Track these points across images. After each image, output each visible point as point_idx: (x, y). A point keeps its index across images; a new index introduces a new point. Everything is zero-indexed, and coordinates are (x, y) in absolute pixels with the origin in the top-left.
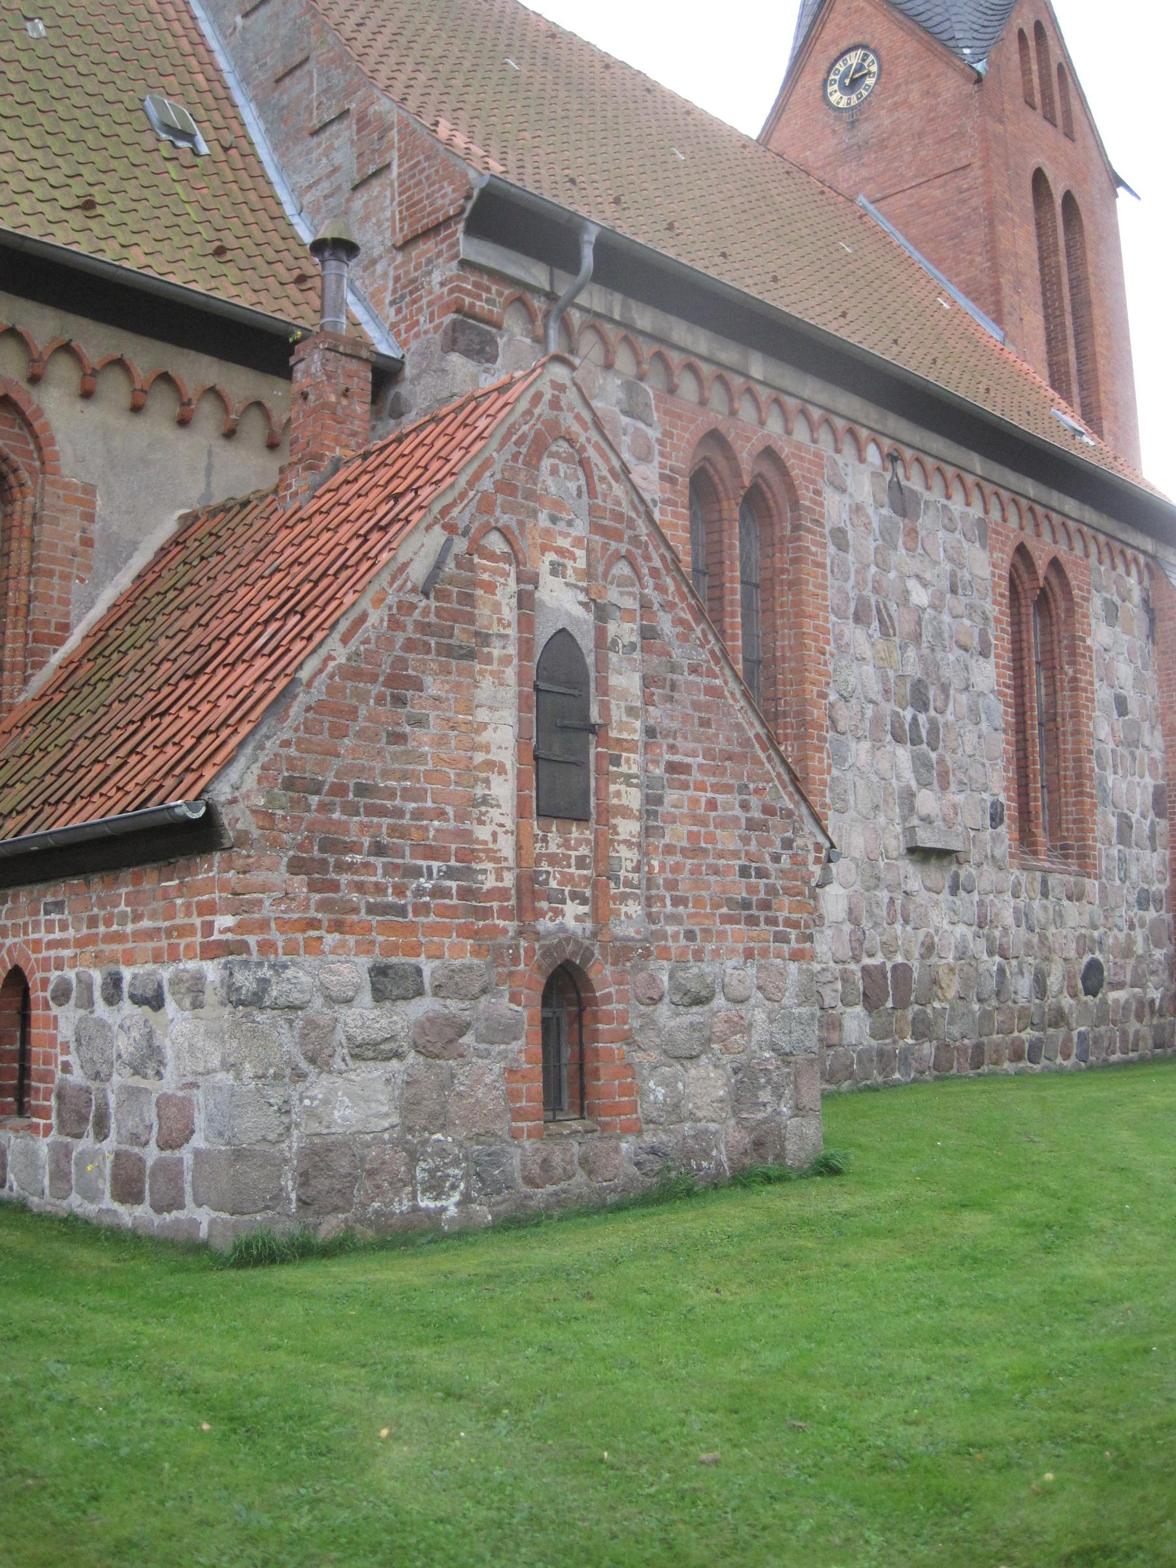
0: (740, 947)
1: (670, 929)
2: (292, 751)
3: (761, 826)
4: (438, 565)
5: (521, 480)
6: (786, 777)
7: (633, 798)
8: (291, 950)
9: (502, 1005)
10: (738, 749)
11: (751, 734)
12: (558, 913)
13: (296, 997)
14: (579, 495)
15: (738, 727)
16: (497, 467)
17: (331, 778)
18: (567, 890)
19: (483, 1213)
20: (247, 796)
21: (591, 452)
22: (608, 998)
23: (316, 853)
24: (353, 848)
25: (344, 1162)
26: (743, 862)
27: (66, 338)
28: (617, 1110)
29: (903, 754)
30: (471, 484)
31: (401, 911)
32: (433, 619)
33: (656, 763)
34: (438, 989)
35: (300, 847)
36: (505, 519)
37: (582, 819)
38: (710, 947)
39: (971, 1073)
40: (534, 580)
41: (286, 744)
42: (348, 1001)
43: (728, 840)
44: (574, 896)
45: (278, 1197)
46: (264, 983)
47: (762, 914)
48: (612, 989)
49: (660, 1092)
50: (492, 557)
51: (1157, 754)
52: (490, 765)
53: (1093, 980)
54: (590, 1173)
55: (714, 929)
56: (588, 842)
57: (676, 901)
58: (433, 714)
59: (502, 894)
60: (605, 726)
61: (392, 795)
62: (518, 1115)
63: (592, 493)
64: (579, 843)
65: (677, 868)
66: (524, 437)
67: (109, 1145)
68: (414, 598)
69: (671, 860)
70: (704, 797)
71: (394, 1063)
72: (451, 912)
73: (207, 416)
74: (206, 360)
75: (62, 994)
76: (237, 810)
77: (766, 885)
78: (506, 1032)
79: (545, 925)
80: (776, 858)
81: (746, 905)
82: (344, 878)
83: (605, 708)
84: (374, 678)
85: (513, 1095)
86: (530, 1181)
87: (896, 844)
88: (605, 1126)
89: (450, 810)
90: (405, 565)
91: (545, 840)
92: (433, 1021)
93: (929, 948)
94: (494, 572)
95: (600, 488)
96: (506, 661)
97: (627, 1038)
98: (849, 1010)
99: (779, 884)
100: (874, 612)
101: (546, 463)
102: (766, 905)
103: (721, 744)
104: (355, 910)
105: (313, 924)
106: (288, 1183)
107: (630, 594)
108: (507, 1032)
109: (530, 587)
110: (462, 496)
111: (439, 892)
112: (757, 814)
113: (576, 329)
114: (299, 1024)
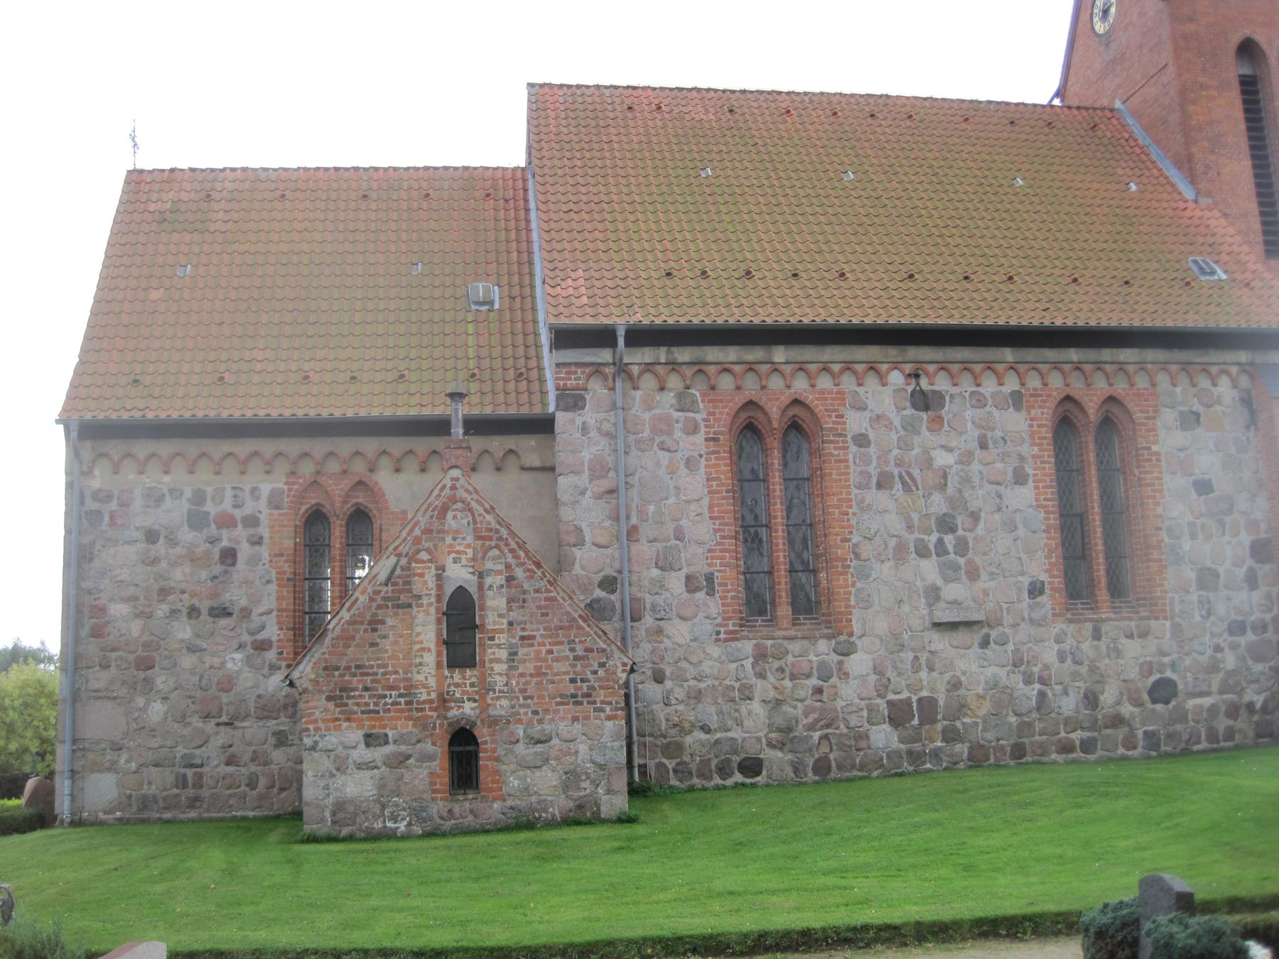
0: (570, 716)
1: (522, 711)
2: (327, 656)
4: (393, 572)
5: (436, 526)
6: (601, 633)
7: (503, 654)
8: (328, 729)
9: (428, 747)
11: (576, 615)
13: (330, 747)
14: (469, 524)
15: (568, 613)
16: (422, 524)
17: (344, 664)
19: (418, 830)
20: (307, 675)
21: (474, 504)
23: (338, 693)
26: (572, 676)
27: (383, 448)
28: (491, 790)
30: (409, 534)
31: (378, 712)
32: (390, 594)
33: (514, 637)
34: (395, 742)
35: (331, 691)
36: (427, 545)
37: (472, 665)
38: (548, 717)
39: (1012, 763)
40: (443, 568)
41: (324, 653)
42: (354, 747)
43: (559, 667)
44: (469, 700)
45: (323, 820)
46: (316, 743)
47: (585, 700)
48: (488, 738)
50: (422, 562)
52: (423, 649)
54: (475, 816)
55: (551, 709)
56: (476, 676)
57: (525, 698)
59: (431, 701)
60: (483, 625)
61: (372, 667)
62: (434, 791)
63: (475, 522)
64: (471, 677)
65: (527, 683)
66: (436, 507)
68: (380, 588)
69: (523, 680)
70: (544, 650)
71: (376, 771)
72: (402, 711)
79: (452, 713)
80: (595, 672)
81: (574, 696)
82: (350, 702)
83: (482, 617)
84: (362, 623)
85: (432, 783)
86: (441, 818)
89: (400, 671)
90: (376, 575)
91: (452, 677)
94: (424, 568)
95: (479, 519)
96: (430, 604)
97: (497, 759)
98: (874, 728)
100: (897, 478)
101: (450, 515)
103: (556, 622)
104: (356, 713)
105: (337, 719)
106: (328, 814)
108: (431, 758)
109: (441, 572)
110: (404, 540)
112: (580, 653)
113: (636, 376)
114: (332, 757)
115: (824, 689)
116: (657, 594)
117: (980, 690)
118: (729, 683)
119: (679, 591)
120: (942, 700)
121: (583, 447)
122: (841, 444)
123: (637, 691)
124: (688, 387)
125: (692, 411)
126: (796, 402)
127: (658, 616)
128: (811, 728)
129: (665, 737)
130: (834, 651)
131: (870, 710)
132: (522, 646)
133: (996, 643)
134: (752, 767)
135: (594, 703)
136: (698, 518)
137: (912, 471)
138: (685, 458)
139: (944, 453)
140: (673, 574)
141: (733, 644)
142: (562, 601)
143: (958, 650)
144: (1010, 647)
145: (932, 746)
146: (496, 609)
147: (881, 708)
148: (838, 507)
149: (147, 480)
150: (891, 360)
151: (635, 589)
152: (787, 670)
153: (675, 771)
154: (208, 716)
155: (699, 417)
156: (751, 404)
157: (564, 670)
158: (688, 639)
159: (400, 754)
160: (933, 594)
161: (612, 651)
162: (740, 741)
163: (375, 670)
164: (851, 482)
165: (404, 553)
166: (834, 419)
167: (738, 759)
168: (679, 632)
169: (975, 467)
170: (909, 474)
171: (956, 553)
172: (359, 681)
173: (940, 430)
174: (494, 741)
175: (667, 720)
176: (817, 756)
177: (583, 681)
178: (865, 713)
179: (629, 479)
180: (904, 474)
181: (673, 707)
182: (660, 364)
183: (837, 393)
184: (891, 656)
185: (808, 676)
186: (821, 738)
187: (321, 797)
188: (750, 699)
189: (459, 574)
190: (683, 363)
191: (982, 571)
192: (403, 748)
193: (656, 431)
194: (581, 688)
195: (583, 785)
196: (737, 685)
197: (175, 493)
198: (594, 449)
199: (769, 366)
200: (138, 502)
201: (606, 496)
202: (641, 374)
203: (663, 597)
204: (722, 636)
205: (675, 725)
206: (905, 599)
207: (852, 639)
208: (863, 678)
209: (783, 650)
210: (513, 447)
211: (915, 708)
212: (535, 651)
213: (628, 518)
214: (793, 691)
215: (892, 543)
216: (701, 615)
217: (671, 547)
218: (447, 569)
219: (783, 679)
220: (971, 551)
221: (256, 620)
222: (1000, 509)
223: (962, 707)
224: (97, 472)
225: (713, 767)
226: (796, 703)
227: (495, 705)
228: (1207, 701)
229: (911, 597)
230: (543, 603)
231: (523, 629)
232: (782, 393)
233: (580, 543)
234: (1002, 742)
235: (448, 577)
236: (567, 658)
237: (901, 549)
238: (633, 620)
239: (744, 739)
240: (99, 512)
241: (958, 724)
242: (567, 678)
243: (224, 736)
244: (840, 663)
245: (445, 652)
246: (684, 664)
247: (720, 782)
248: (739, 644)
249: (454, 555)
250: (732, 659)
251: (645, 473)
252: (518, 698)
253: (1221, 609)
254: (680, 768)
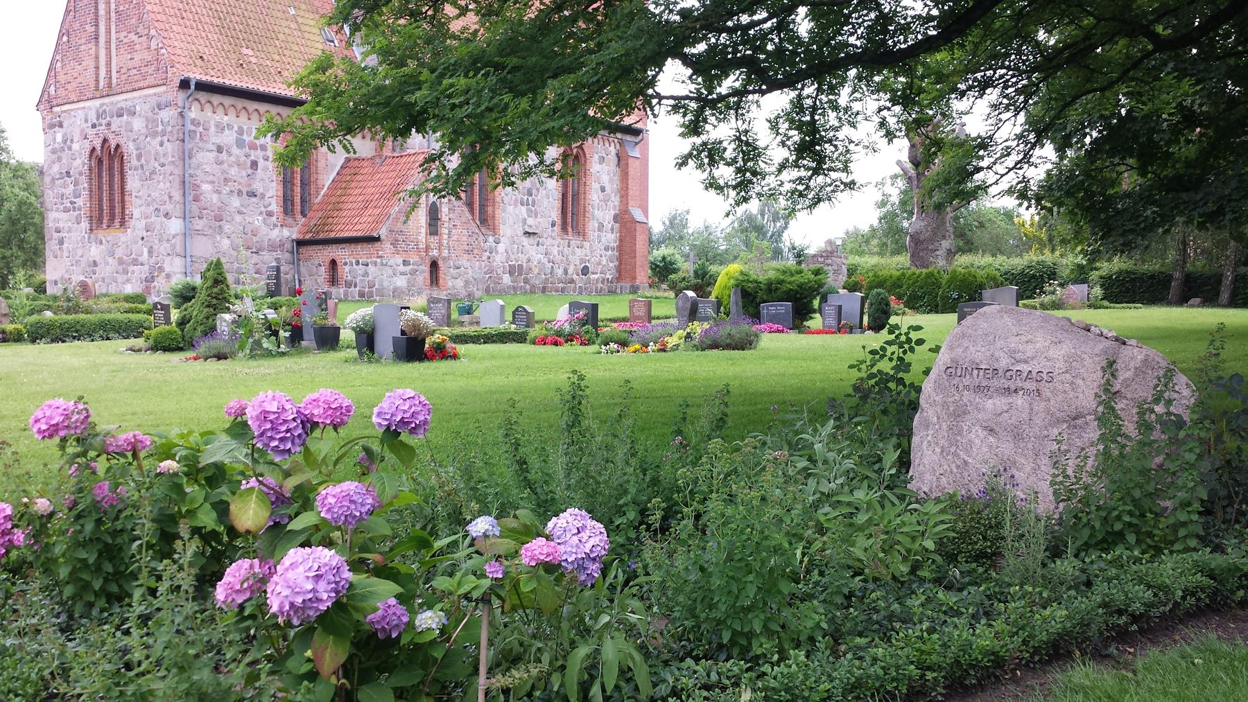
7: (446, 231)
29: (524, 209)
51: (617, 203)
53: (585, 271)
67: (358, 289)
75: (345, 264)
78: (423, 272)
87: (520, 232)
92: (412, 270)
93: (529, 261)
103: (464, 220)
154: (248, 248)
197: (230, 127)
200: (213, 129)
221: (267, 200)
224: (193, 109)
228: (596, 276)
243: (255, 258)
253: (603, 240)
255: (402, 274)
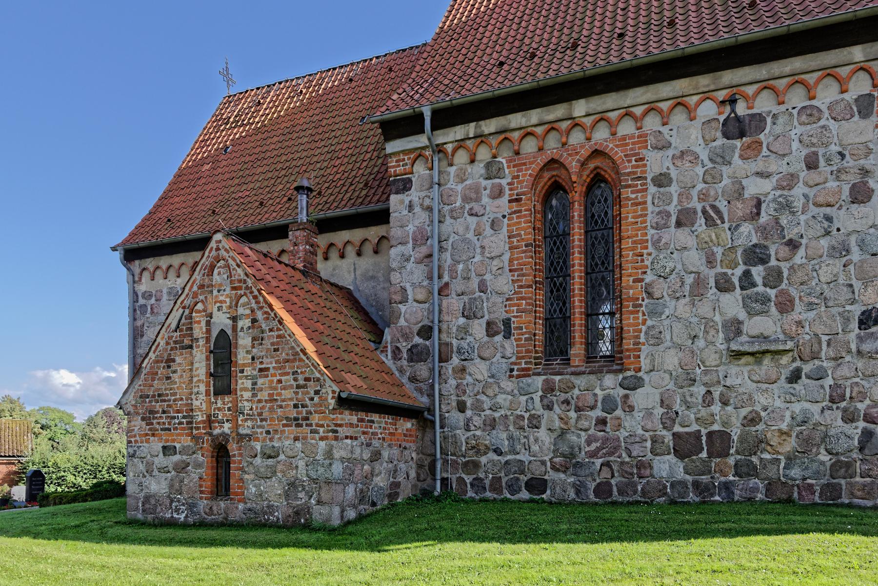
0: (292, 436)
1: (259, 430)
2: (142, 387)
3: (305, 387)
7: (248, 384)
10: (292, 357)
12: (222, 427)
18: (225, 419)
22: (234, 456)
24: (157, 412)
25: (153, 501)
26: (295, 402)
28: (236, 494)
30: (190, 290)
35: (144, 414)
36: (201, 297)
37: (229, 392)
38: (277, 436)
41: (140, 385)
43: (288, 394)
45: (137, 509)
47: (304, 423)
49: (254, 490)
57: (262, 420)
58: (178, 369)
61: (167, 395)
62: (201, 492)
64: (228, 402)
65: (263, 408)
68: (172, 334)
69: (260, 405)
70: (275, 379)
72: (183, 429)
73: (350, 251)
74: (344, 232)
76: (127, 406)
77: (306, 411)
80: (312, 399)
81: (296, 419)
82: (155, 421)
84: (162, 362)
85: (201, 486)
88: (232, 499)
89: (184, 397)
90: (170, 324)
91: (216, 403)
95: (233, 273)
97: (242, 469)
98: (658, 458)
99: (312, 410)
100: (700, 214)
101: (216, 271)
102: (307, 419)
105: (147, 435)
107: (247, 308)
109: (209, 318)
111: (180, 423)
112: (302, 382)
115: (608, 420)
116: (462, 339)
117: (784, 427)
118: (520, 413)
119: (481, 336)
120: (735, 433)
121: (408, 221)
122: (639, 187)
123: (442, 418)
124: (495, 157)
125: (499, 178)
126: (597, 153)
127: (462, 357)
128: (593, 454)
129: (465, 457)
130: (620, 385)
131: (654, 441)
132: (261, 377)
133: (808, 377)
134: (537, 485)
135: (311, 425)
136: (500, 271)
137: (717, 204)
138: (490, 220)
139: (759, 180)
140: (476, 321)
141: (524, 380)
142: (288, 338)
143: (760, 385)
144: (829, 381)
145: (723, 479)
146: (245, 347)
147: (666, 441)
148: (633, 249)
149: (169, 283)
150: (700, 90)
151: (444, 336)
152: (573, 402)
153: (471, 484)
155: (504, 182)
156: (553, 162)
157: (289, 397)
158: (486, 375)
159: (183, 461)
160: (734, 328)
161: (324, 380)
162: (527, 463)
163: (169, 397)
164: (648, 224)
165: (187, 306)
166: (634, 163)
167: (526, 479)
168: (479, 370)
169: (799, 190)
170: (713, 207)
171: (765, 285)
172: (160, 406)
173: (757, 156)
174: (241, 455)
175: (467, 443)
176: (598, 481)
177: (303, 406)
178: (649, 444)
179: (444, 244)
180: (708, 208)
181: (472, 433)
182: (470, 138)
183: (639, 136)
184: (680, 391)
185: (592, 408)
186: (602, 465)
187: (137, 492)
188: (537, 428)
189: (221, 320)
190: (490, 134)
191: (797, 301)
192: (185, 457)
193: (466, 199)
194: (301, 413)
195: (300, 495)
196: (527, 415)
198: (417, 223)
199: (569, 122)
201: (425, 260)
202: (455, 151)
203: (468, 341)
204: (515, 373)
205: (473, 448)
206: (701, 335)
207: (640, 374)
208: (649, 413)
209: (570, 385)
210: (385, 234)
211: (704, 442)
212: (269, 381)
213: (440, 277)
214: (577, 421)
215: (689, 280)
216: (499, 355)
217: (475, 299)
218: (213, 316)
219: (568, 411)
220: (785, 281)
222: (828, 233)
223: (761, 442)
225: (504, 484)
226: (580, 432)
227: (244, 426)
229: (707, 332)
230: (275, 340)
231: (261, 363)
232: (582, 147)
233: (404, 301)
234: (809, 481)
235: (214, 323)
236: (291, 386)
237: (699, 284)
238: (441, 361)
239: (530, 462)
240: (145, 306)
241: (754, 459)
242: (292, 403)
244: (626, 397)
245: (212, 382)
246: (483, 398)
247: (509, 496)
248: (529, 380)
249: (218, 304)
250: (523, 393)
251: (457, 237)
252: (256, 420)
254: (476, 482)
255: (164, 470)
